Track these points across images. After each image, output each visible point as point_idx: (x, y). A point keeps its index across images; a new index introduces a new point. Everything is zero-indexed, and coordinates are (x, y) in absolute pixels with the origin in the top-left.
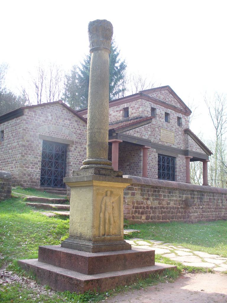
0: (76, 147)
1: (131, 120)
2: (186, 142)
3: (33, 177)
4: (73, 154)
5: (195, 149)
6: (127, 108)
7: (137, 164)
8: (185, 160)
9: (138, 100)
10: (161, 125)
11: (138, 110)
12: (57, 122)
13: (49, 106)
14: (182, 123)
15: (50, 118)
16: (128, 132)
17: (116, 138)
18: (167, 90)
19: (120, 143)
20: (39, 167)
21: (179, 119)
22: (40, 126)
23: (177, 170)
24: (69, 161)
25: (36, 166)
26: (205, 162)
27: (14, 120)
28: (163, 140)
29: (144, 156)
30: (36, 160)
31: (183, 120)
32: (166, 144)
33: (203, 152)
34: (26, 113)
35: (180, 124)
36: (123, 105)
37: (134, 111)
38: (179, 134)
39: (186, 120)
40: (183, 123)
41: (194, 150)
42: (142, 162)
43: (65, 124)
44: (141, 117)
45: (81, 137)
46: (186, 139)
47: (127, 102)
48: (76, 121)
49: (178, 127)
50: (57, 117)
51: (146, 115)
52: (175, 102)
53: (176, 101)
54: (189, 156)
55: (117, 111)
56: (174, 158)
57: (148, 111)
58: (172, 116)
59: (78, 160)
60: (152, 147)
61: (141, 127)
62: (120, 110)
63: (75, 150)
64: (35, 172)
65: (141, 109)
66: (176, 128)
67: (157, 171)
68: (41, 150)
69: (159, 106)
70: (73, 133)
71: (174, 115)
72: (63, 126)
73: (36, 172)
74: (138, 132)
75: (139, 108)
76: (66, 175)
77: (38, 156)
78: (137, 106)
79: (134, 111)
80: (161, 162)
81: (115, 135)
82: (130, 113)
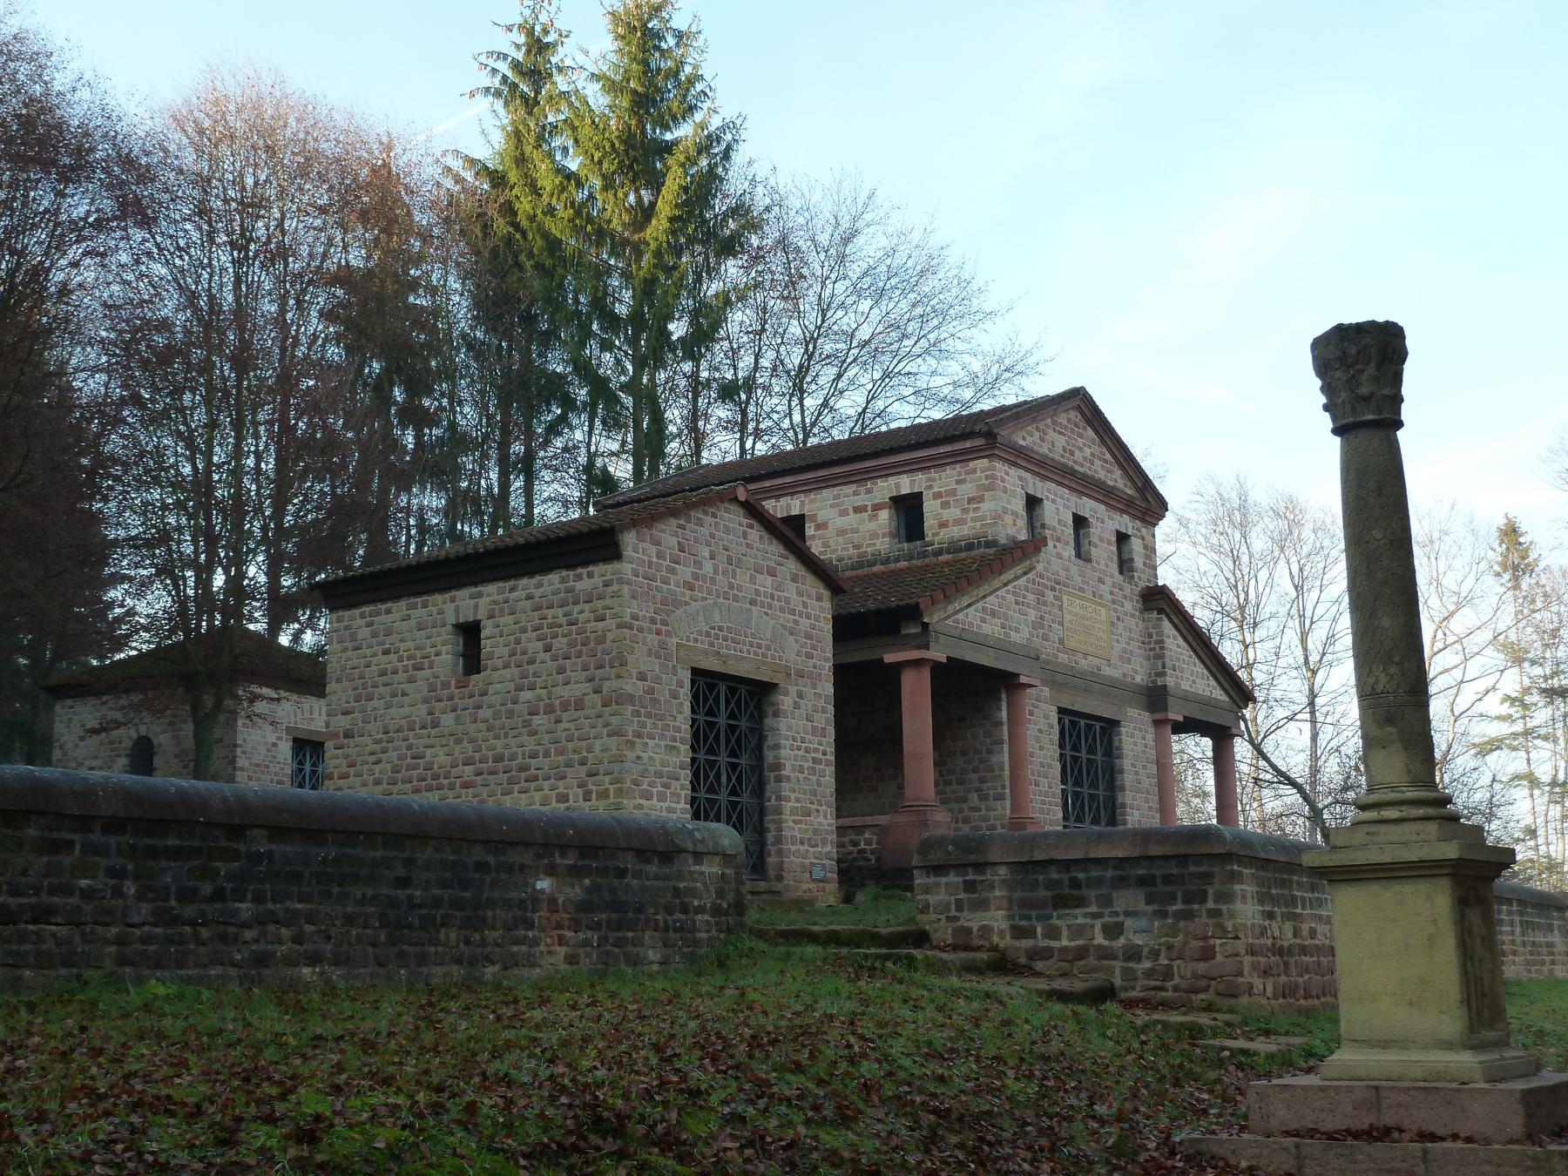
1: (939, 552)
4: (790, 728)
5: (1190, 678)
7: (982, 761)
9: (972, 464)
10: (1063, 576)
12: (731, 587)
14: (1132, 560)
15: (708, 567)
16: (960, 616)
17: (919, 647)
18: (1078, 408)
19: (936, 667)
20: (683, 793)
21: (1122, 538)
22: (677, 604)
23: (1128, 779)
24: (777, 757)
26: (1222, 737)
27: (554, 577)
29: (1013, 721)
31: (1136, 545)
32: (1084, 664)
33: (1219, 695)
34: (628, 552)
35: (1125, 565)
36: (892, 480)
37: (953, 513)
38: (1126, 614)
39: (1146, 547)
40: (1139, 562)
41: (1185, 686)
42: (1006, 747)
43: (758, 593)
44: (989, 544)
45: (814, 647)
46: (1150, 636)
48: (795, 579)
49: (1119, 578)
50: (730, 559)
51: (1011, 531)
52: (1105, 461)
53: (1108, 456)
54: (1172, 716)
55: (858, 510)
56: (1111, 726)
57: (1015, 514)
58: (1098, 532)
59: (807, 751)
60: (1045, 682)
61: (1001, 593)
62: (877, 507)
63: (797, 706)
65: (985, 506)
66: (1114, 585)
67: (1058, 788)
69: (1052, 486)
71: (1106, 523)
72: (753, 602)
74: (993, 614)
75: (981, 499)
78: (967, 490)
79: (953, 513)
80: (1084, 750)
81: (912, 631)
82: (929, 522)
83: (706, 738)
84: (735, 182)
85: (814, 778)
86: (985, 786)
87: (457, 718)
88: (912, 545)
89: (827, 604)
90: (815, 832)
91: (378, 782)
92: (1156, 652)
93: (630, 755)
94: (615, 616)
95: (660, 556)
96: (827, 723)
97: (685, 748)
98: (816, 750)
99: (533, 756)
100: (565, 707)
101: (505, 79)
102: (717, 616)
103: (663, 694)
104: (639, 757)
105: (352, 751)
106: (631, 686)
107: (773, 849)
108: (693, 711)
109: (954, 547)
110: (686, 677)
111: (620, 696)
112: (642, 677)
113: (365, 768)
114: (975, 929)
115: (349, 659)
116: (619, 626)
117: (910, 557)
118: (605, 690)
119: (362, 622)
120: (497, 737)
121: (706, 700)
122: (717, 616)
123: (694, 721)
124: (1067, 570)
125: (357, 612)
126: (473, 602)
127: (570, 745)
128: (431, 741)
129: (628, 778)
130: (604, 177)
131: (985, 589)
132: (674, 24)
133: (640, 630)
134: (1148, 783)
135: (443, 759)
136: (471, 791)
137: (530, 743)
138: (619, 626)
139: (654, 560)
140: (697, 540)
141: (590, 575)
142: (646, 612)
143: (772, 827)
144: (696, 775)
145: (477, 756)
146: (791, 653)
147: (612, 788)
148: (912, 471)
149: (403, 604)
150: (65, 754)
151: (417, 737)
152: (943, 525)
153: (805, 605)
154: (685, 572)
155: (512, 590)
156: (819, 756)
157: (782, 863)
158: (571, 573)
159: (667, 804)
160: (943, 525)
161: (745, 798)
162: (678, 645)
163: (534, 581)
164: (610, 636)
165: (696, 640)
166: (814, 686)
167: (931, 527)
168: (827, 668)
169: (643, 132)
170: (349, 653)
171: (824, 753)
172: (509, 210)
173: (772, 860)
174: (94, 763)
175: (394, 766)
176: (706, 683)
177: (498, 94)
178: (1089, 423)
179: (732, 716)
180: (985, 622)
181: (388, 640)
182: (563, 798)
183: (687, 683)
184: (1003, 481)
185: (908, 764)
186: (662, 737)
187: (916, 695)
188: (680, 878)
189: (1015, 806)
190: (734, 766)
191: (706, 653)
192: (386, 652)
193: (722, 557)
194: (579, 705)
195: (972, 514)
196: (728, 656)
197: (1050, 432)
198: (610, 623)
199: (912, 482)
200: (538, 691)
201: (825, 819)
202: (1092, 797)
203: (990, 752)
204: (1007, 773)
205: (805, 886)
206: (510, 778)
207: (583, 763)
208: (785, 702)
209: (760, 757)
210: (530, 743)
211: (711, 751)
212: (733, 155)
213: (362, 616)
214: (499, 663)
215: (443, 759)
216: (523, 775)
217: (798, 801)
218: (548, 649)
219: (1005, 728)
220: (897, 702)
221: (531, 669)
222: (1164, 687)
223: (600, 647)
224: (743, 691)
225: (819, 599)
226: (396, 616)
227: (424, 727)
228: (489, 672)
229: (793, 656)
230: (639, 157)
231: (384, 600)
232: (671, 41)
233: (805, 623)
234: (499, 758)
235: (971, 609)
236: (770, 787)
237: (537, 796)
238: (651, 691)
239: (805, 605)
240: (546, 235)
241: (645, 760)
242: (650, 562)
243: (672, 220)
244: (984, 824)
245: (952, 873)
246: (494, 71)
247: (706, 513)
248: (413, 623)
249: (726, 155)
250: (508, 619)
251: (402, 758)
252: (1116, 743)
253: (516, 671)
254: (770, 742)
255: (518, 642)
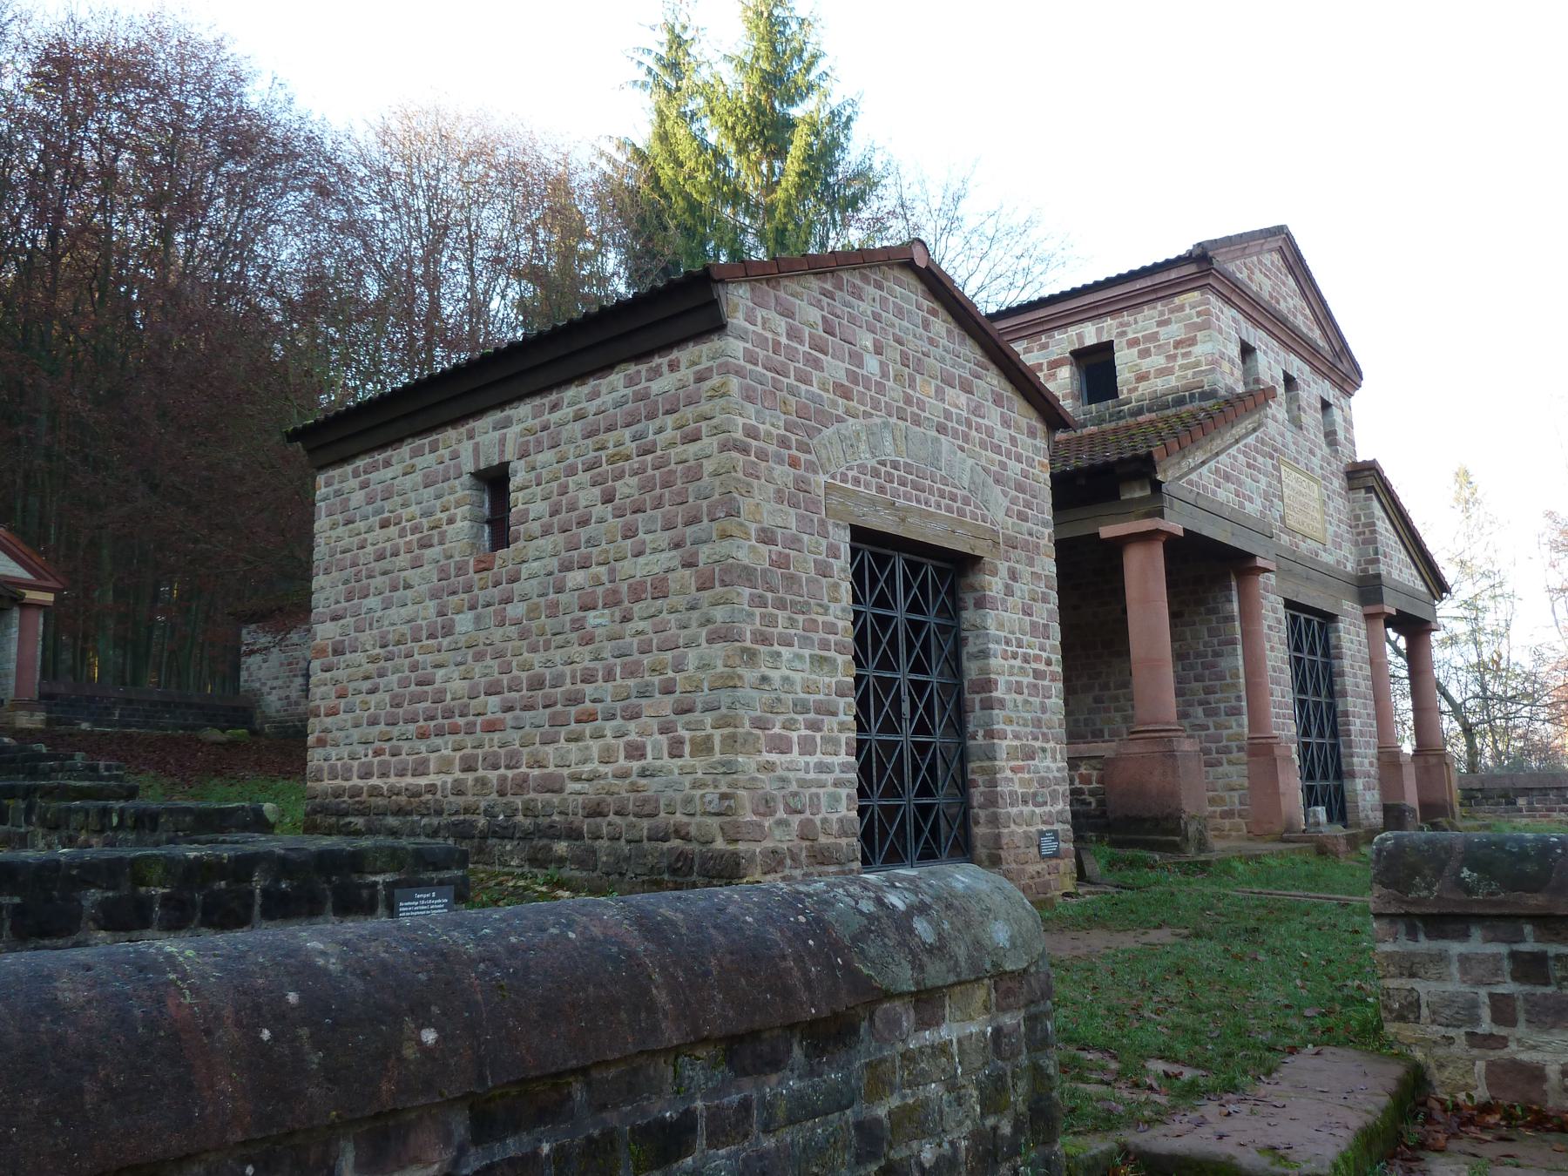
0: (1013, 575)
2: (1359, 534)
3: (817, 819)
4: (1001, 626)
5: (1399, 570)
6: (1106, 349)
8: (1363, 626)
9: (1177, 300)
11: (1185, 355)
12: (908, 400)
13: (858, 282)
15: (872, 364)
16: (1194, 476)
17: (1148, 515)
20: (843, 737)
21: (1326, 405)
22: (825, 419)
24: (985, 670)
25: (825, 732)
27: (617, 378)
28: (1296, 526)
30: (827, 680)
32: (1305, 547)
33: (1420, 586)
34: (737, 320)
36: (1073, 331)
37: (1157, 361)
39: (1345, 420)
44: (1205, 396)
45: (1028, 505)
46: (1357, 518)
47: (1094, 313)
48: (998, 401)
51: (1230, 381)
56: (1329, 619)
63: (1009, 591)
64: (823, 776)
65: (1199, 350)
66: (1323, 458)
68: (844, 604)
70: (991, 481)
71: (1314, 388)
72: (941, 429)
73: (829, 778)
74: (1227, 477)
75: (1192, 342)
76: (971, 766)
77: (832, 654)
78: (1175, 331)
79: (1157, 361)
81: (1138, 494)
82: (1124, 375)
83: (877, 642)
84: (851, 157)
85: (1036, 700)
86: (1212, 697)
87: (478, 619)
88: (1102, 406)
89: (1042, 443)
90: (1042, 782)
91: (373, 722)
92: (1366, 538)
93: (749, 675)
94: (717, 430)
95: (793, 334)
96: (1050, 618)
97: (844, 660)
98: (1037, 658)
99: (588, 678)
100: (637, 595)
101: (650, 71)
102: (888, 446)
103: (804, 567)
104: (764, 679)
105: (339, 674)
106: (746, 552)
107: (983, 815)
108: (856, 600)
109: (1158, 403)
110: (843, 540)
111: (727, 570)
112: (767, 537)
113: (358, 699)
114: (1553, 1071)
115: (339, 539)
116: (724, 448)
117: (1100, 420)
118: (702, 558)
119: (353, 483)
120: (534, 650)
121: (874, 581)
122: (888, 446)
123: (857, 614)
124: (1282, 435)
125: (349, 469)
126: (497, 434)
127: (647, 660)
128: (443, 656)
129: (746, 716)
130: (738, 142)
131: (1217, 444)
132: (797, 13)
133: (762, 455)
134: (1365, 686)
135: (458, 686)
136: (496, 736)
137: (583, 657)
138: (724, 448)
139: (784, 340)
140: (852, 320)
141: (673, 367)
142: (772, 424)
143: (979, 779)
144: (862, 703)
145: (505, 679)
146: (998, 510)
147: (717, 736)
148: (1099, 316)
149: (406, 449)
150: (250, 675)
151: (426, 651)
152: (1142, 378)
153: (1013, 441)
154: (836, 368)
155: (555, 407)
156: (1042, 667)
157: (998, 837)
158: (643, 368)
159: (818, 757)
160: (1142, 378)
161: (937, 738)
162: (828, 486)
163: (585, 389)
164: (709, 467)
165: (857, 481)
166: (1031, 563)
167: (1126, 382)
168: (1045, 535)
169: (772, 107)
170: (340, 530)
171: (1049, 663)
172: (654, 179)
173: (980, 831)
174: (275, 683)
175: (393, 698)
176: (874, 551)
177: (644, 85)
178: (1291, 270)
179: (914, 607)
180: (1216, 487)
181: (388, 505)
182: (635, 752)
183: (845, 550)
184: (1218, 319)
185: (1139, 677)
186: (806, 642)
187: (1145, 577)
188: (879, 1084)
189: (1255, 723)
190: (919, 687)
191: (873, 502)
192: (384, 525)
193: (893, 352)
194: (660, 590)
195: (1180, 361)
196: (908, 509)
197: (1257, 271)
198: (709, 443)
199: (1099, 331)
200: (595, 569)
201: (1053, 764)
202: (1317, 704)
203: (1217, 654)
204: (1242, 681)
205: (1031, 869)
206: (553, 717)
207: (668, 690)
208: (994, 585)
209: (957, 671)
210: (583, 657)
211: (885, 664)
212: (852, 124)
213: (356, 474)
214: (535, 527)
215: (458, 686)
216: (573, 710)
217: (1016, 737)
218: (608, 499)
219: (1237, 624)
220: (1119, 592)
221: (583, 534)
222: (1378, 576)
223: (691, 487)
224: (929, 569)
225: (1032, 434)
226: (397, 468)
227: (431, 636)
228: (520, 544)
229: (1001, 516)
230: (767, 131)
231: (383, 447)
232: (794, 26)
233: (1015, 467)
234: (537, 684)
235: (1204, 469)
236: (974, 719)
237: (595, 747)
238: (782, 562)
239: (1013, 441)
240: (687, 197)
241: (777, 684)
242: (777, 344)
243: (801, 174)
244: (1213, 746)
245: (1476, 933)
246: (640, 63)
247: (866, 279)
248: (418, 477)
249: (847, 125)
250: (548, 456)
251: (404, 683)
252: (1333, 641)
253: (559, 538)
254: (971, 648)
255: (563, 491)
